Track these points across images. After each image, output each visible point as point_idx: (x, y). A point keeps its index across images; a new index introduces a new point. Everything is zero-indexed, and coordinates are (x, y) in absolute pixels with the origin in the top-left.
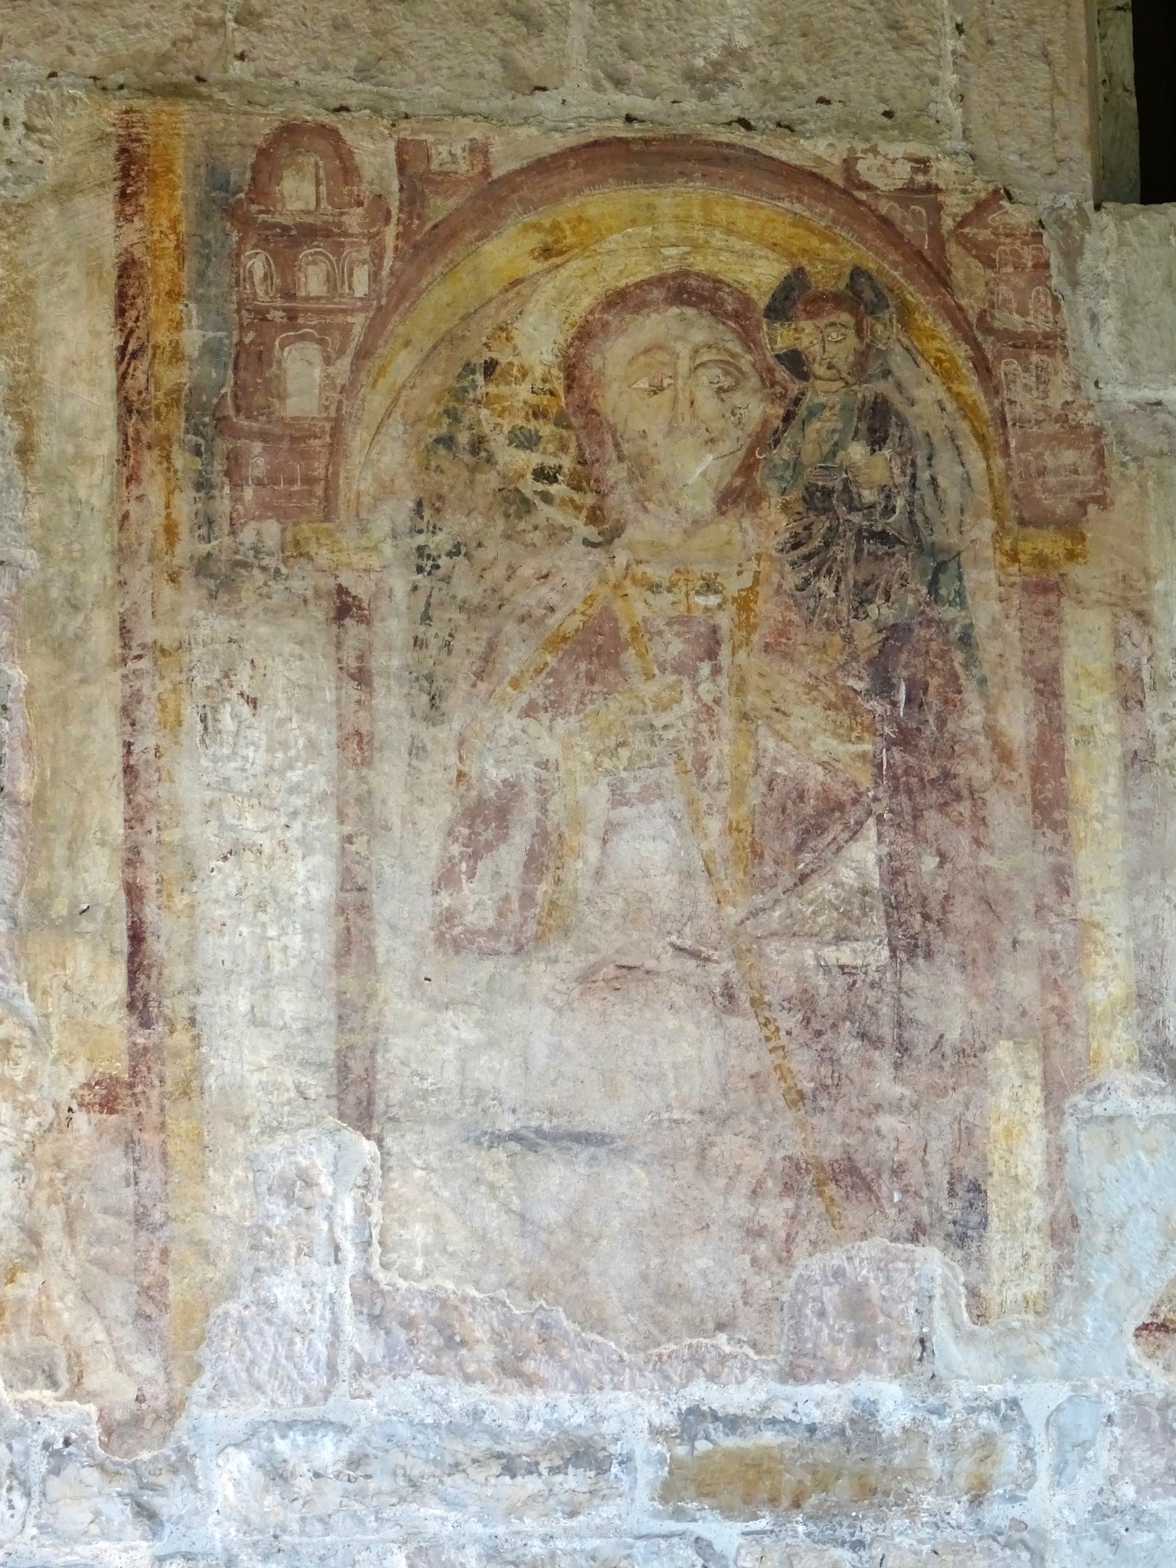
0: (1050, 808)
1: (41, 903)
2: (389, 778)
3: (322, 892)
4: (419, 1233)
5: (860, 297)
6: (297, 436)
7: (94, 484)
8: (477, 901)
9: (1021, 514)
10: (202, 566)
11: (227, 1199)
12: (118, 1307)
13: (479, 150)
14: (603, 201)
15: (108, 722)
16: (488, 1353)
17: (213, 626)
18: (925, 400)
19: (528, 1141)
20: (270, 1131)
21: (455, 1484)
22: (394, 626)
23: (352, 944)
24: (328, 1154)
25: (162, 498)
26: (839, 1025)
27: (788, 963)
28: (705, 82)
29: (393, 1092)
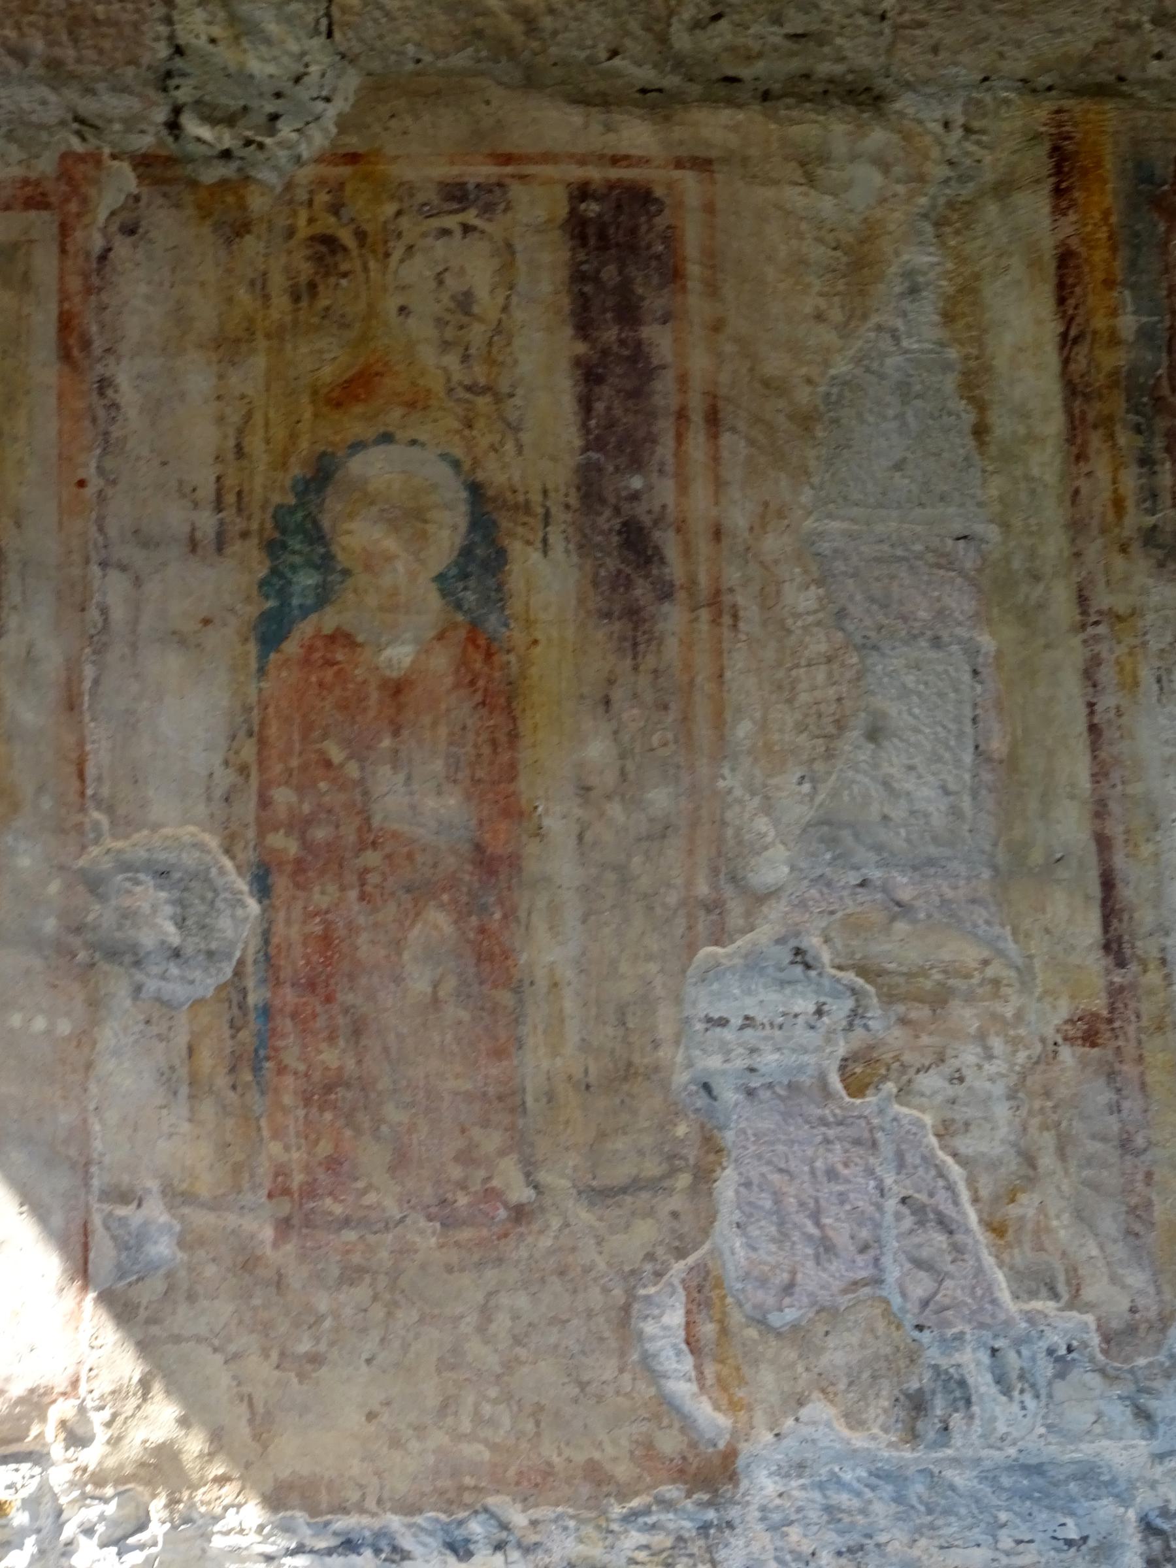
7: (1045, 463)
12: (1109, 1226)
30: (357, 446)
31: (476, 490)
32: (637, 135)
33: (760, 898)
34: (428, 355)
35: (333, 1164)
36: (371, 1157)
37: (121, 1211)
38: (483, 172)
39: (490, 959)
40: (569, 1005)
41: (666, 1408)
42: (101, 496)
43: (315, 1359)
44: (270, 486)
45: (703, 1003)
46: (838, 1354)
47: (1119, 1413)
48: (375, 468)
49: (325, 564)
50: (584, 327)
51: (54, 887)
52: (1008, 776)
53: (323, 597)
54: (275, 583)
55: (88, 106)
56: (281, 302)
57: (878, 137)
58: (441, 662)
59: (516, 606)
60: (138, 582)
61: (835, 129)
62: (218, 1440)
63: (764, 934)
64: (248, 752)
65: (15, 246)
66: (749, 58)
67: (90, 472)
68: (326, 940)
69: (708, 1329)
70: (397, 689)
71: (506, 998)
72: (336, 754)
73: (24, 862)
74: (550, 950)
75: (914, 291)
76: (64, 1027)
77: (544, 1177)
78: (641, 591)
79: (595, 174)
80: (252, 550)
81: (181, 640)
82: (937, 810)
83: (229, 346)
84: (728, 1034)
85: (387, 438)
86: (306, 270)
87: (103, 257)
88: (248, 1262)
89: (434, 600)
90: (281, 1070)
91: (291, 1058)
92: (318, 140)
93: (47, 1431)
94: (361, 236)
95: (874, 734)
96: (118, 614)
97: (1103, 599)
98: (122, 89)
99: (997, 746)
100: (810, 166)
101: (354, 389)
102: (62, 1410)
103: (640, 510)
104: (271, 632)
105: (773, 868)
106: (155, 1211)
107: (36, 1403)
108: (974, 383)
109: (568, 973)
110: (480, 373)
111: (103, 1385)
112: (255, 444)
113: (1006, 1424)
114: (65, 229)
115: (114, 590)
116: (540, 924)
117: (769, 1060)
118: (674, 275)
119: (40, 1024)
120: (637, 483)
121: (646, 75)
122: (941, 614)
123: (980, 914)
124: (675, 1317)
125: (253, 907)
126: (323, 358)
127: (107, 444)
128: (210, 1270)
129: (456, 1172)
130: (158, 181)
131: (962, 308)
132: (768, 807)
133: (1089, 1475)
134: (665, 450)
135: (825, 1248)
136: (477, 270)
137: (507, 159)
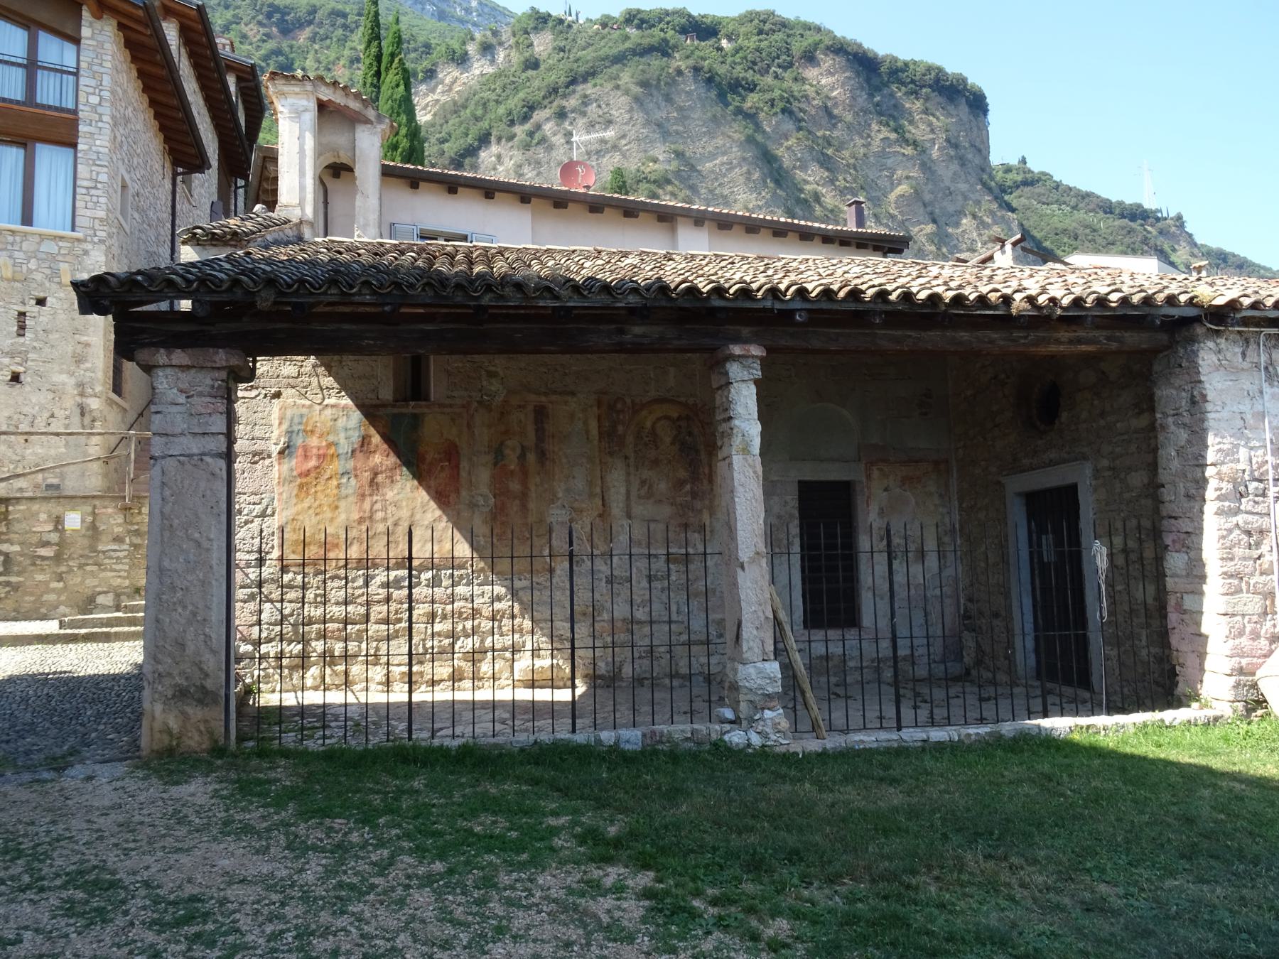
7: (596, 442)
32: (543, 399)
39: (524, 507)
48: (509, 443)
52: (591, 484)
61: (569, 398)
74: (532, 505)
100: (566, 403)
104: (495, 464)
105: (560, 495)
108: (587, 432)
115: (475, 459)
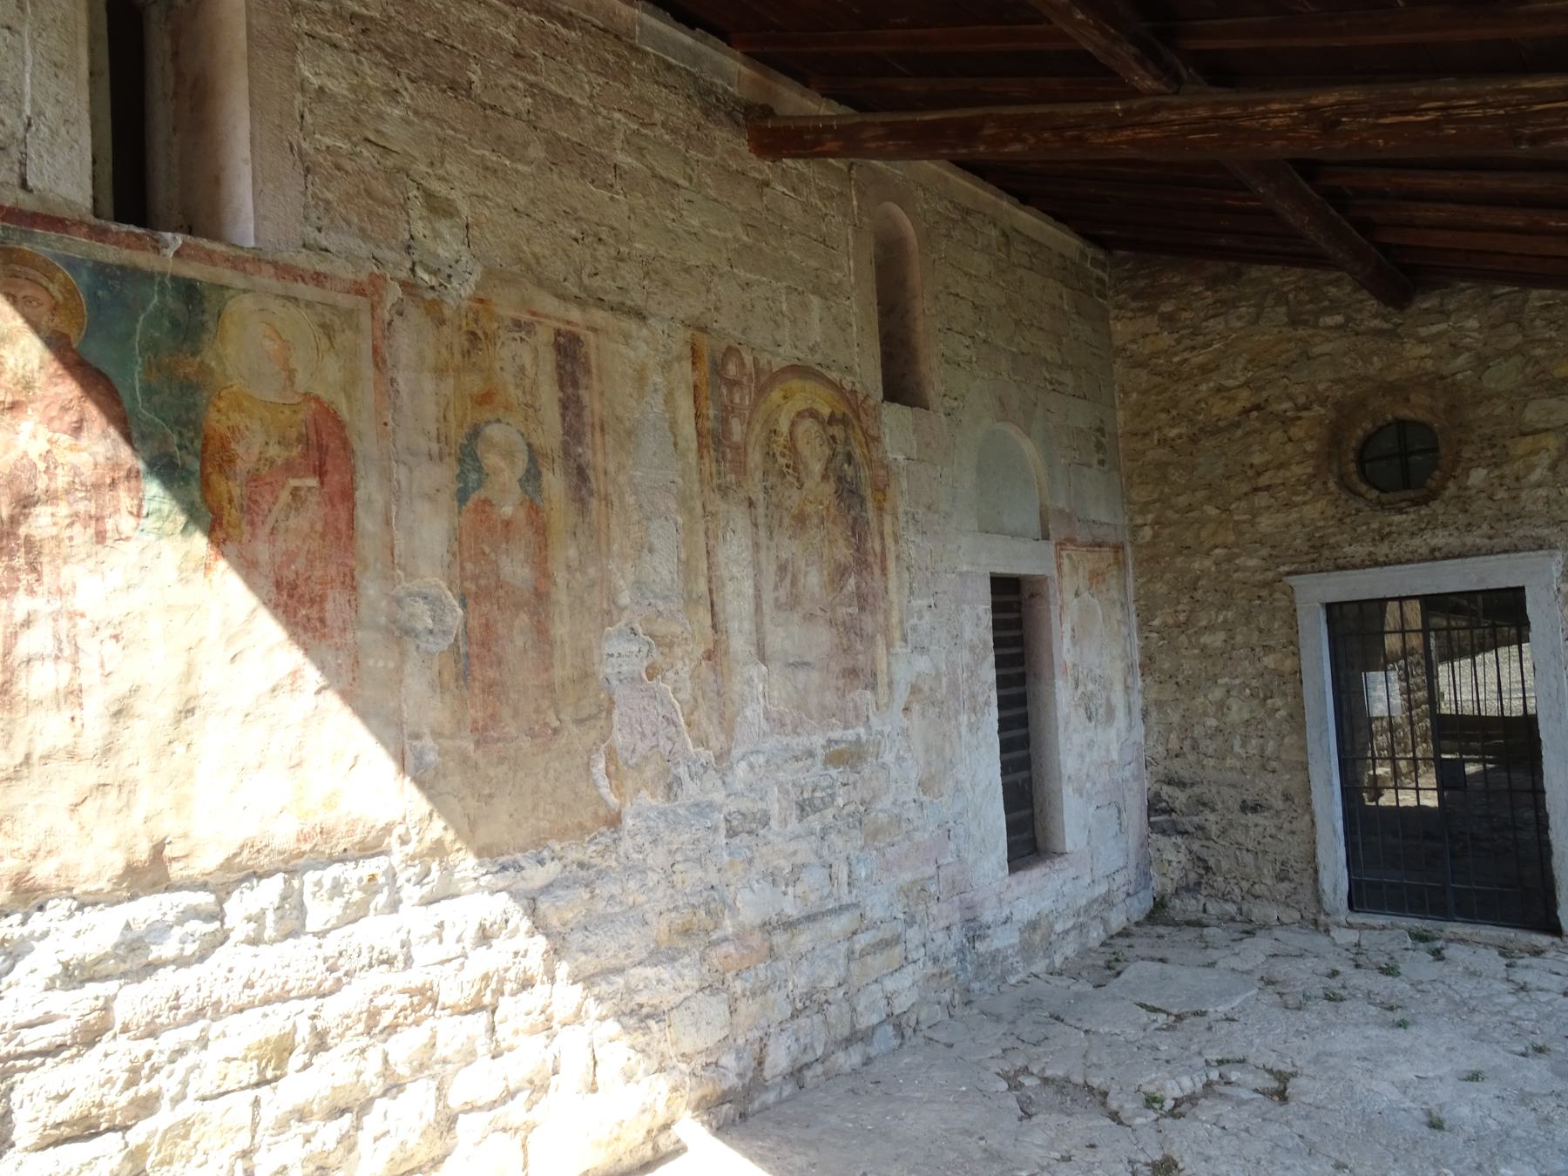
0: (884, 570)
1: (690, 593)
2: (763, 555)
3: (750, 591)
4: (775, 694)
5: (844, 421)
6: (736, 448)
7: (692, 457)
8: (782, 594)
9: (877, 489)
10: (719, 486)
11: (736, 686)
12: (715, 721)
13: (769, 363)
14: (795, 384)
15: (702, 534)
16: (790, 727)
17: (723, 507)
18: (858, 452)
19: (795, 665)
20: (745, 664)
21: (786, 766)
22: (761, 510)
23: (758, 608)
24: (756, 671)
25: (709, 466)
26: (850, 631)
27: (842, 612)
28: (812, 350)
29: (769, 652)
30: (488, 423)
31: (529, 445)
32: (575, 314)
33: (622, 609)
34: (511, 389)
35: (493, 716)
36: (506, 713)
37: (415, 743)
38: (525, 317)
39: (541, 631)
40: (567, 650)
41: (601, 800)
42: (394, 431)
43: (491, 796)
44: (458, 436)
45: (607, 649)
46: (649, 772)
47: (719, 783)
49: (479, 470)
50: (562, 387)
51: (384, 603)
52: (686, 567)
53: (480, 484)
54: (462, 476)
55: (378, 254)
56: (458, 356)
57: (645, 332)
58: (522, 514)
59: (545, 494)
60: (411, 470)
61: (631, 325)
62: (459, 833)
63: (622, 623)
64: (456, 547)
65: (352, 311)
66: (607, 293)
67: (389, 419)
68: (487, 625)
69: (612, 768)
70: (507, 524)
71: (547, 648)
72: (487, 550)
73: (371, 592)
74: (560, 629)
75: (656, 391)
76: (391, 665)
77: (562, 716)
78: (584, 492)
79: (563, 327)
80: (452, 461)
81: (430, 498)
82: (668, 578)
83: (440, 372)
84: (613, 660)
85: (498, 421)
86: (466, 345)
87: (390, 324)
88: (464, 759)
89: (518, 490)
90: (474, 679)
91: (477, 674)
92: (467, 291)
93: (392, 841)
94: (486, 334)
95: (651, 551)
96: (404, 484)
97: (710, 508)
98: (391, 249)
99: (683, 556)
101: (485, 399)
102: (399, 830)
103: (582, 461)
104: (462, 496)
105: (625, 599)
106: (428, 742)
107: (388, 829)
109: (566, 638)
110: (529, 399)
111: (416, 818)
112: (451, 416)
113: (691, 789)
114: (373, 307)
116: (556, 618)
117: (625, 668)
118: (588, 372)
119: (381, 664)
120: (580, 450)
121: (575, 291)
122: (668, 509)
123: (681, 615)
124: (602, 765)
125: (460, 611)
126: (474, 384)
127: (396, 409)
128: (451, 764)
129: (534, 717)
130: (410, 294)
131: (669, 399)
132: (623, 577)
133: (710, 805)
134: (588, 439)
135: (643, 735)
136: (527, 359)
137: (534, 314)
